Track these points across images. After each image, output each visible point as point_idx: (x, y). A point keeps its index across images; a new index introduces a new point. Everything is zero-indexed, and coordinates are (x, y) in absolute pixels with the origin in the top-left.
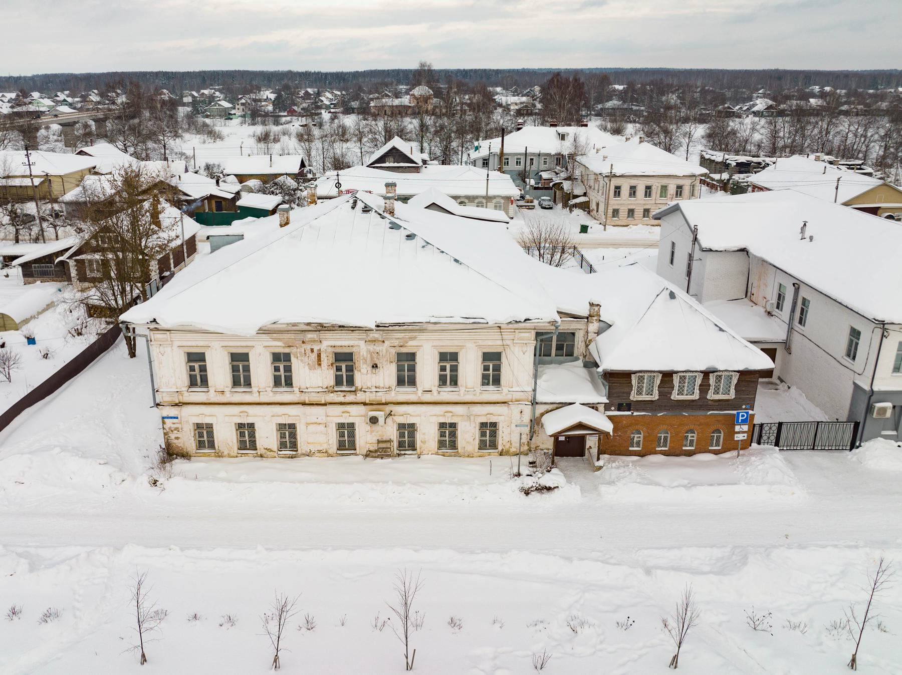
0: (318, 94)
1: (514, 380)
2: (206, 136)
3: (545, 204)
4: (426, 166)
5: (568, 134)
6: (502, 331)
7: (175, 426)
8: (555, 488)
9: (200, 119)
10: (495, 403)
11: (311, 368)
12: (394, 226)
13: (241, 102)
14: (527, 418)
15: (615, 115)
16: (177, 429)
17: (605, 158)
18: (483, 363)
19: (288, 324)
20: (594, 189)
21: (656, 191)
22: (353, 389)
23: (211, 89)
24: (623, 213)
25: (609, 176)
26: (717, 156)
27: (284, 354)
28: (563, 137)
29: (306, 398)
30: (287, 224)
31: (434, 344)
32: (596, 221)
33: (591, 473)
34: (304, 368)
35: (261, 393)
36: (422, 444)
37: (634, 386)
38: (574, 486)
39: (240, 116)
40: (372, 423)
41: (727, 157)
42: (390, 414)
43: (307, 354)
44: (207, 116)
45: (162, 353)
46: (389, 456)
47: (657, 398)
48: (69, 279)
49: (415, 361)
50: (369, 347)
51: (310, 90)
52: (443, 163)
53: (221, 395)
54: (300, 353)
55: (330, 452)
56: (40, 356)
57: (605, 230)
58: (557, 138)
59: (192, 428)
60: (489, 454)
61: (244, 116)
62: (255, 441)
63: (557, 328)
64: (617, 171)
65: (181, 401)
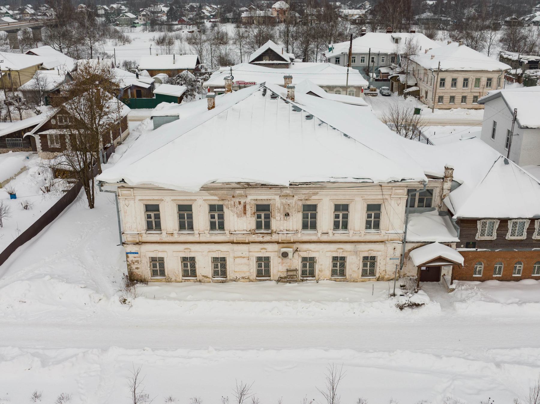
0: (200, 8)
1: (390, 225)
2: (117, 40)
3: (385, 92)
4: (294, 63)
5: (400, 39)
6: (382, 188)
7: (136, 259)
8: (422, 304)
9: (112, 27)
10: (375, 242)
11: (239, 216)
12: (296, 109)
13: (142, 14)
14: (398, 253)
15: (428, 24)
16: (137, 262)
17: (432, 57)
18: (366, 212)
19: (223, 183)
20: (424, 81)
21: (471, 83)
22: (269, 231)
23: (118, 4)
24: (446, 99)
25: (437, 71)
26: (513, 56)
27: (218, 205)
28: (397, 41)
29: (235, 238)
30: (213, 107)
31: (331, 198)
32: (425, 105)
33: (446, 294)
34: (233, 216)
35: (201, 235)
36: (320, 273)
37: (479, 229)
38: (435, 303)
39: (142, 25)
40: (284, 257)
41: (521, 56)
42: (296, 251)
43: (236, 205)
44: (117, 25)
45: (127, 205)
46: (296, 281)
47: (495, 238)
48: (35, 149)
49: (316, 210)
50: (282, 201)
51: (194, 5)
52: (304, 61)
53: (170, 236)
54: (231, 205)
55: (251, 278)
56: (21, 207)
57: (433, 112)
58: (392, 42)
59: (255, 260)
60: (369, 280)
61: (145, 25)
62: (195, 270)
63: (425, 186)
64: (443, 67)
65: (141, 240)
